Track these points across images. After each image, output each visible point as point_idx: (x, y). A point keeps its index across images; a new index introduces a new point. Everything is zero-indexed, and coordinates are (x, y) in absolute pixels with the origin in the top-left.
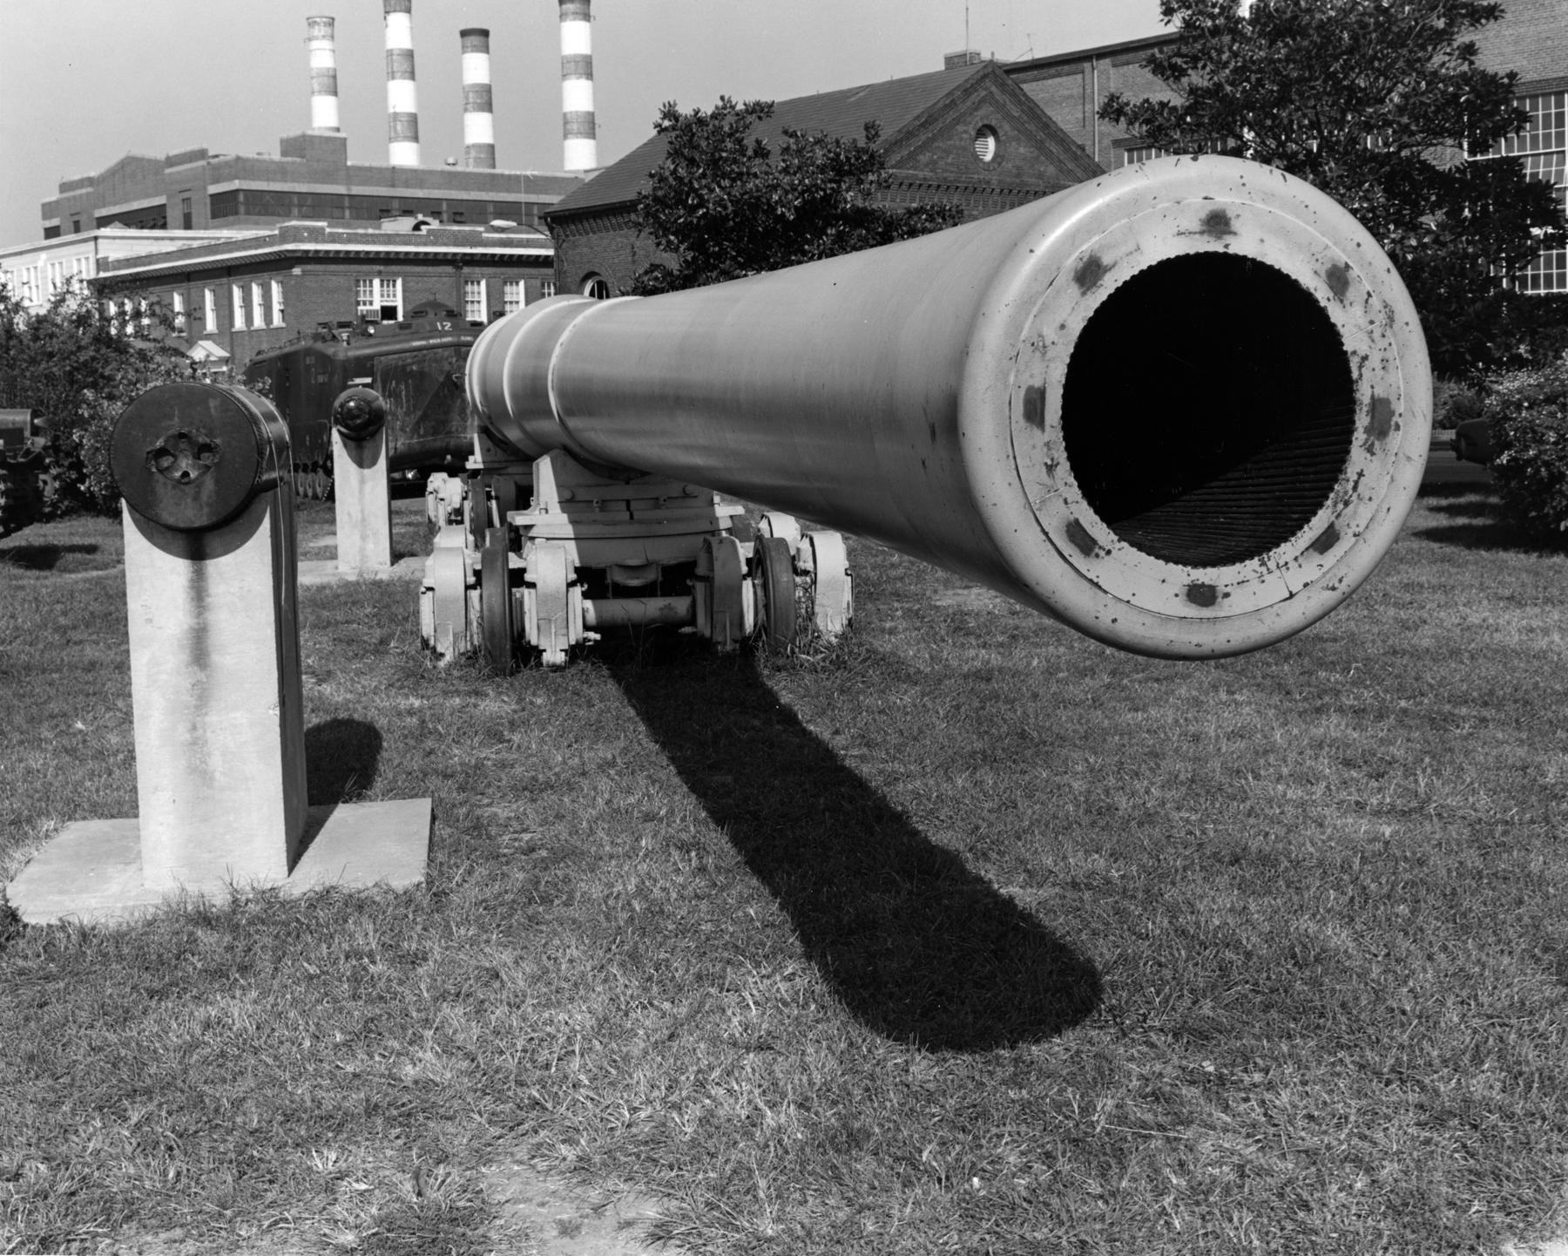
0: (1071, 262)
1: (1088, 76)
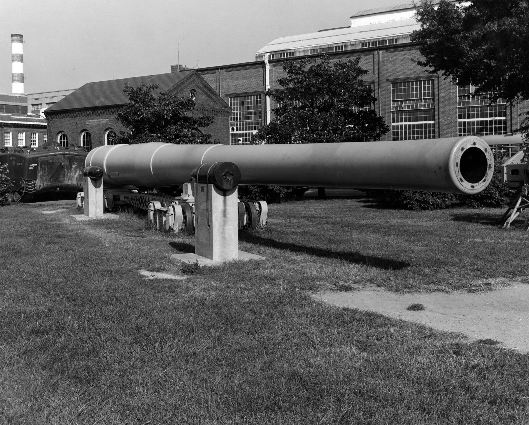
0: (461, 148)
1: (217, 74)
